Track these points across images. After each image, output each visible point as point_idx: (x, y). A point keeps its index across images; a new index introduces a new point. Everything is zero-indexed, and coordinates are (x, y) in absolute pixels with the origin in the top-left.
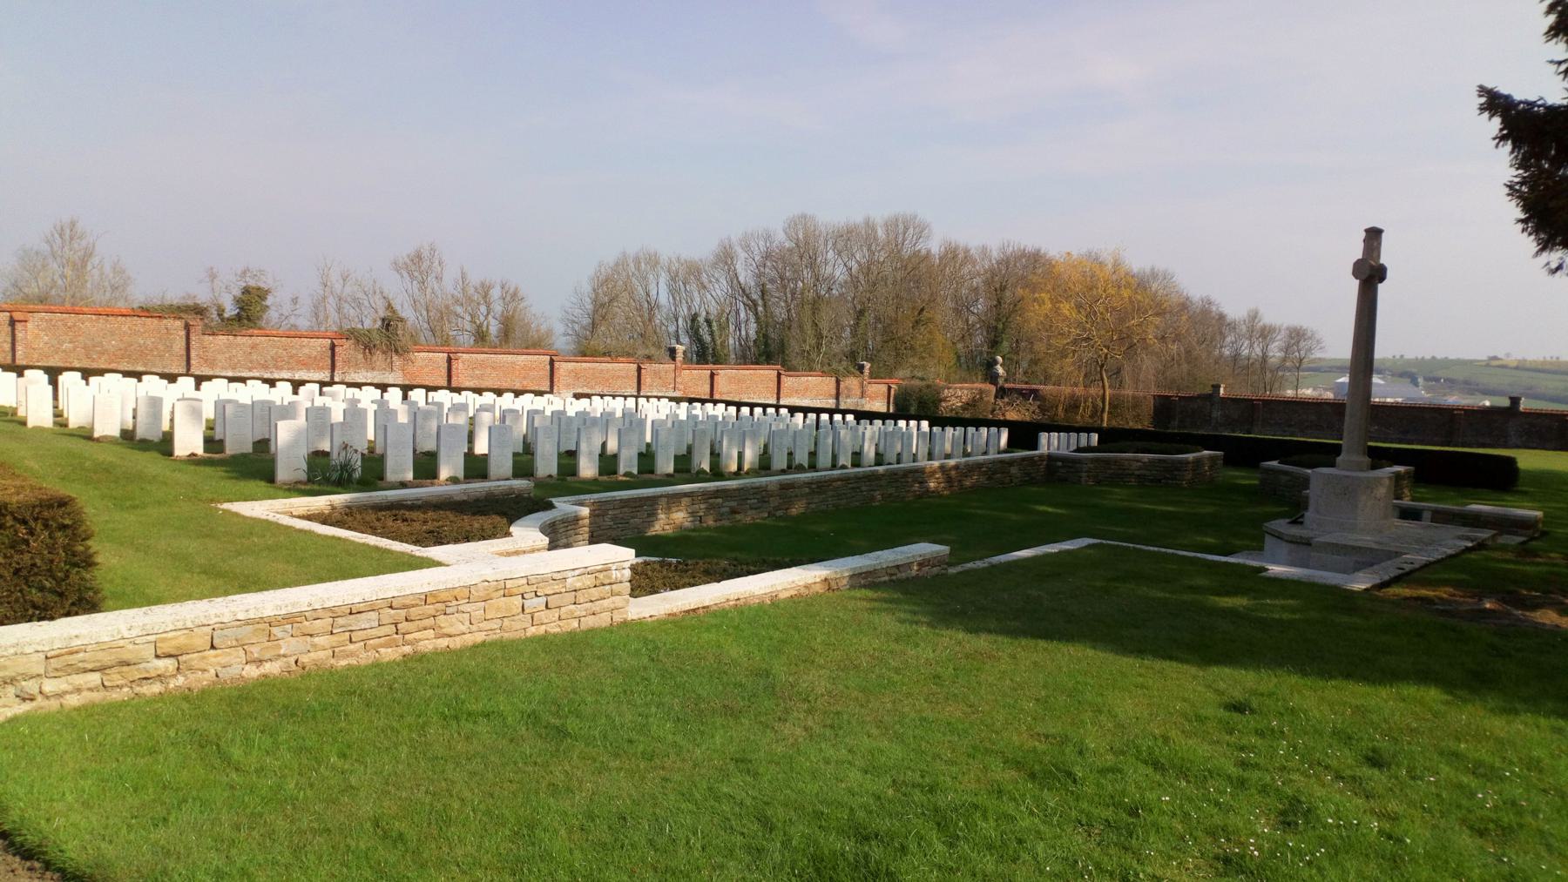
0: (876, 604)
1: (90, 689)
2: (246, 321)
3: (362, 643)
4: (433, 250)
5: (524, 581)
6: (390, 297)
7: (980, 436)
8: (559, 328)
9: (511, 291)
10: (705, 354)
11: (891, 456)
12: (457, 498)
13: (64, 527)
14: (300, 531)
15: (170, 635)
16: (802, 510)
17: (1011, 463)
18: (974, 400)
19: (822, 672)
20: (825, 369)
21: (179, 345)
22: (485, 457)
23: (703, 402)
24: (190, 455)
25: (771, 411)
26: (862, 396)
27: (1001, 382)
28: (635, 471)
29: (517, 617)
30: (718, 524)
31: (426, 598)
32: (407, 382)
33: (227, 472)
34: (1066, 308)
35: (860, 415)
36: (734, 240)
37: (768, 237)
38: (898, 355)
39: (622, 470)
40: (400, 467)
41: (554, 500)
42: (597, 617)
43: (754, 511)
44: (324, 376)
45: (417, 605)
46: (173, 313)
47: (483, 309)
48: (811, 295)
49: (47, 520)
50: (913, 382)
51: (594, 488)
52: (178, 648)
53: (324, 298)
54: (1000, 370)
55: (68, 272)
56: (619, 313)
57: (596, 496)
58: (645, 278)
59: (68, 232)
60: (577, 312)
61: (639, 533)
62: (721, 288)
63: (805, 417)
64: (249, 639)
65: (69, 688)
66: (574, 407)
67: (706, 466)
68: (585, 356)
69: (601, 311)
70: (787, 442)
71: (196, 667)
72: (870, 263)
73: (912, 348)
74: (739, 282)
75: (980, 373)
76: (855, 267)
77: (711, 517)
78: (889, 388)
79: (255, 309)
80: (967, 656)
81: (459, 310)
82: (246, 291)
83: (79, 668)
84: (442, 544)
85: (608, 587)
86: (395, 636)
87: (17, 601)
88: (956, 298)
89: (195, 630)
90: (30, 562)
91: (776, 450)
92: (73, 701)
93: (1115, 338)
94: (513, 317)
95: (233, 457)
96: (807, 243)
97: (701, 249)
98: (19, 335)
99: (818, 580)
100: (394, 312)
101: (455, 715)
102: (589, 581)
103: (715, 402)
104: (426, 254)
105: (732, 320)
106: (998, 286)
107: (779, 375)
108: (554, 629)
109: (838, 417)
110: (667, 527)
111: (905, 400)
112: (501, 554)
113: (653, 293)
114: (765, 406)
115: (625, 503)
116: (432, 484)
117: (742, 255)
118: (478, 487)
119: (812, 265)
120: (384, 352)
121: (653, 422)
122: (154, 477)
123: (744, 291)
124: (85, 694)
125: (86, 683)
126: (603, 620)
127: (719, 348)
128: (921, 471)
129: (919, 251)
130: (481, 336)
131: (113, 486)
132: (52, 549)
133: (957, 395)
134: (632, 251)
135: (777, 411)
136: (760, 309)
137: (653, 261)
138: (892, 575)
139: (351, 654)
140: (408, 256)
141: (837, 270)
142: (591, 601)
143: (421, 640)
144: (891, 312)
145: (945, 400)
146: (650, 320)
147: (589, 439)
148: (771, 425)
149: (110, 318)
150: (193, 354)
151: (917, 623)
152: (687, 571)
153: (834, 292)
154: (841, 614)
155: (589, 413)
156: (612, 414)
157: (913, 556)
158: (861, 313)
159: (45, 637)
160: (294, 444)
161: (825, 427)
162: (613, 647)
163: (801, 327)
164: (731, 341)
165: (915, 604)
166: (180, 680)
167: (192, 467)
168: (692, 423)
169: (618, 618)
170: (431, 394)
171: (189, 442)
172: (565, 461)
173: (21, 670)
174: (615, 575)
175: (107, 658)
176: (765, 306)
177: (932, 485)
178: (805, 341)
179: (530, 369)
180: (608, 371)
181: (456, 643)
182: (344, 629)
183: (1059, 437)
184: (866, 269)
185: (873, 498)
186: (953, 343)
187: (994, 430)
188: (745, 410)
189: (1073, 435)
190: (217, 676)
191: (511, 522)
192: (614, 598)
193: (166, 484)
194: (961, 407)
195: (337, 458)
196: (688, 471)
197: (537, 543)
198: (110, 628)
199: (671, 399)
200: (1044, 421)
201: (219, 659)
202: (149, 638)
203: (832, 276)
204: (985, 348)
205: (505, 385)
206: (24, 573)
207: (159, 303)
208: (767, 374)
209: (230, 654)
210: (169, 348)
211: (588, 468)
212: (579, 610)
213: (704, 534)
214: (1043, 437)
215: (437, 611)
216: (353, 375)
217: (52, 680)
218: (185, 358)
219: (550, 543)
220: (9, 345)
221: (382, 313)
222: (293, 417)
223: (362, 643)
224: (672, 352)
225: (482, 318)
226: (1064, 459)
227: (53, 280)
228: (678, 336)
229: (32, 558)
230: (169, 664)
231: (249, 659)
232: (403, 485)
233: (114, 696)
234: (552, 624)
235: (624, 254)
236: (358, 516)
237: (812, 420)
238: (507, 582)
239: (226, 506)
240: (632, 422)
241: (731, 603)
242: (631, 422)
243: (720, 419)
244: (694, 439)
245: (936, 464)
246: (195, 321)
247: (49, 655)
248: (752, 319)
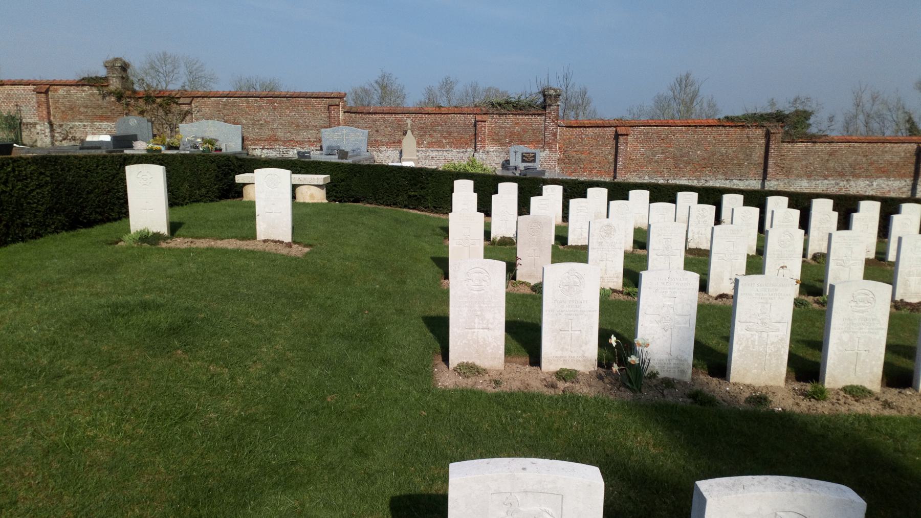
21: (759, 152)
46: (756, 121)
53: (856, 116)
55: (682, 108)
98: (621, 148)
149: (699, 129)
150: (771, 162)
207: (470, 387)
210: (748, 156)
218: (762, 166)
220: (613, 157)
227: (673, 114)
246: (778, 131)
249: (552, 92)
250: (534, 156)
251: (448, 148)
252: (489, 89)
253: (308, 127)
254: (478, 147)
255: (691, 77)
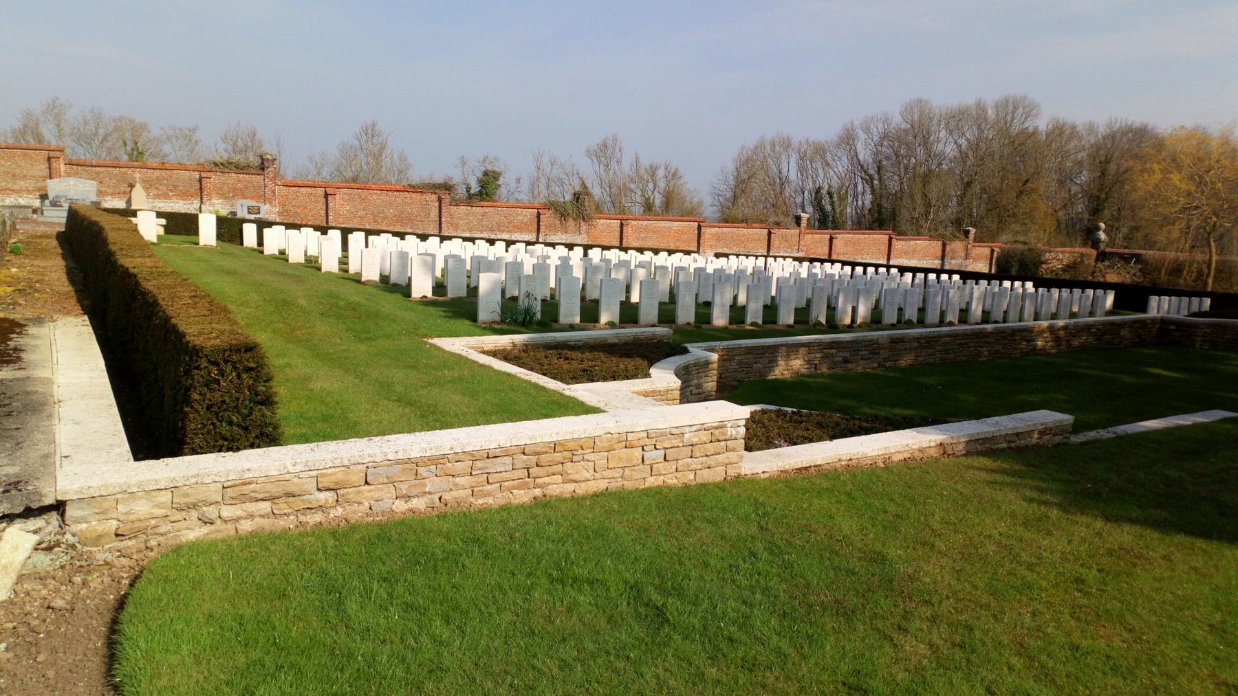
0: (999, 477)
1: (262, 516)
2: (485, 196)
3: (498, 485)
4: (615, 140)
5: (645, 435)
6: (584, 178)
7: (1050, 297)
8: (708, 200)
9: (672, 171)
10: (826, 221)
11: (998, 315)
12: (610, 341)
13: (248, 370)
14: (482, 366)
15: (330, 471)
16: (910, 362)
17: (1122, 325)
18: (1075, 263)
19: (943, 561)
20: (932, 233)
22: (636, 306)
23: (822, 261)
24: (422, 297)
25: (882, 270)
26: (967, 257)
27: (1102, 246)
28: (760, 322)
29: (637, 468)
30: (832, 371)
31: (555, 447)
32: (590, 243)
33: (443, 311)
34: (1175, 178)
35: (966, 276)
36: (856, 123)
37: (886, 120)
38: (1001, 222)
39: (749, 320)
40: (570, 312)
41: (689, 346)
42: (712, 470)
43: (865, 362)
44: (531, 237)
45: (546, 453)
47: (651, 185)
48: (922, 169)
49: (235, 363)
50: (1015, 246)
51: (724, 335)
52: (336, 483)
54: (1102, 236)
55: (370, 159)
56: (756, 188)
57: (725, 343)
58: (779, 158)
59: (370, 132)
60: (723, 187)
61: (761, 376)
62: (842, 165)
63: (914, 277)
64: (399, 477)
65: (244, 514)
66: (713, 265)
67: (823, 320)
68: (727, 222)
69: (741, 186)
70: (898, 300)
71: (353, 500)
72: (979, 140)
73: (1014, 215)
74: (858, 160)
75: (1079, 238)
76: (963, 142)
77: (825, 365)
78: (992, 251)
79: (491, 187)
80: (1110, 552)
81: (633, 186)
82: (486, 174)
83: (251, 497)
84: (593, 381)
85: (723, 443)
86: (527, 479)
87: (209, 432)
88: (1060, 170)
89: (351, 467)
90: (220, 399)
91: (887, 306)
92: (246, 526)
93: (1225, 206)
94: (673, 191)
95: (452, 299)
96: (920, 122)
97: (826, 132)
98: (331, 205)
99: (933, 444)
100: (586, 188)
101: (562, 578)
102: (705, 437)
103: (833, 262)
104: (610, 143)
105: (850, 192)
106: (1103, 159)
107: (890, 239)
108: (672, 481)
109: (944, 277)
110: (786, 372)
111: (1007, 262)
112: (638, 393)
113: (785, 171)
114: (877, 266)
115: (749, 350)
116: (594, 328)
117: (862, 136)
118: (630, 332)
119: (926, 143)
120: (575, 220)
121: (778, 279)
122: (387, 315)
123: (862, 167)
124: (258, 520)
125: (258, 511)
126: (716, 475)
127: (838, 216)
128: (1029, 330)
129: (1027, 128)
130: (648, 207)
131: (356, 321)
132: (239, 389)
133: (1058, 258)
134: (769, 135)
135: (888, 271)
136: (876, 182)
137: (786, 144)
138: (1010, 442)
139: (488, 494)
140: (597, 145)
141: (947, 146)
142: (707, 456)
143: (549, 484)
144: (996, 183)
145: (1045, 262)
146: (781, 193)
147: (722, 294)
148: (882, 284)
149: (390, 193)
150: (443, 220)
151: (1045, 503)
152: (801, 422)
153: (944, 166)
154: (959, 487)
155: (725, 270)
156: (743, 272)
157: (1034, 425)
158: (969, 184)
159: (222, 469)
160: (490, 293)
161: (934, 287)
162: (723, 509)
163: (912, 197)
164: (849, 210)
165: (1043, 480)
166: (339, 511)
167: (421, 307)
168: (812, 280)
169: (732, 472)
170: (605, 252)
171: (422, 287)
172: (701, 310)
173: (201, 497)
174: (730, 432)
175: (275, 490)
176: (880, 180)
177: (1040, 343)
178: (914, 209)
179: (682, 233)
180: (744, 235)
181: (581, 489)
182: (481, 472)
183: (1170, 301)
184: (974, 146)
185: (979, 354)
186: (1056, 211)
187: (1100, 292)
188: (859, 270)
189: (1185, 300)
190: (370, 508)
191: (651, 364)
192: (728, 453)
193: (394, 321)
194: (1062, 268)
195: (523, 303)
196: (806, 323)
197: (671, 385)
198: (277, 463)
199: (795, 259)
200: (1145, 284)
201: (373, 493)
202: (312, 473)
203: (943, 152)
204: (1086, 216)
205: (662, 246)
206: (215, 409)
208: (880, 238)
209: (382, 490)
211: (720, 318)
212: (695, 464)
213: (818, 380)
214: (1154, 301)
215: (565, 459)
216: (552, 236)
217: (229, 507)
219: (683, 383)
221: (578, 189)
222: (498, 271)
223: (498, 485)
224: (798, 220)
225: (650, 193)
226: (1178, 324)
228: (804, 206)
229: (222, 396)
230: (329, 497)
231: (398, 495)
232: (572, 327)
233: (281, 523)
234: (669, 477)
235: (763, 138)
236: (532, 353)
237: (921, 279)
238: (629, 434)
239: (437, 341)
240: (761, 278)
241: (843, 463)
242: (759, 279)
243: (837, 277)
244: (813, 294)
245: (1045, 324)
246: (446, 198)
247: (225, 486)
248: (868, 191)
249: (268, 157)
250: (259, 209)
251: (174, 200)
252: (121, 119)
253: (25, 176)
254: (205, 200)
255: (377, 127)
